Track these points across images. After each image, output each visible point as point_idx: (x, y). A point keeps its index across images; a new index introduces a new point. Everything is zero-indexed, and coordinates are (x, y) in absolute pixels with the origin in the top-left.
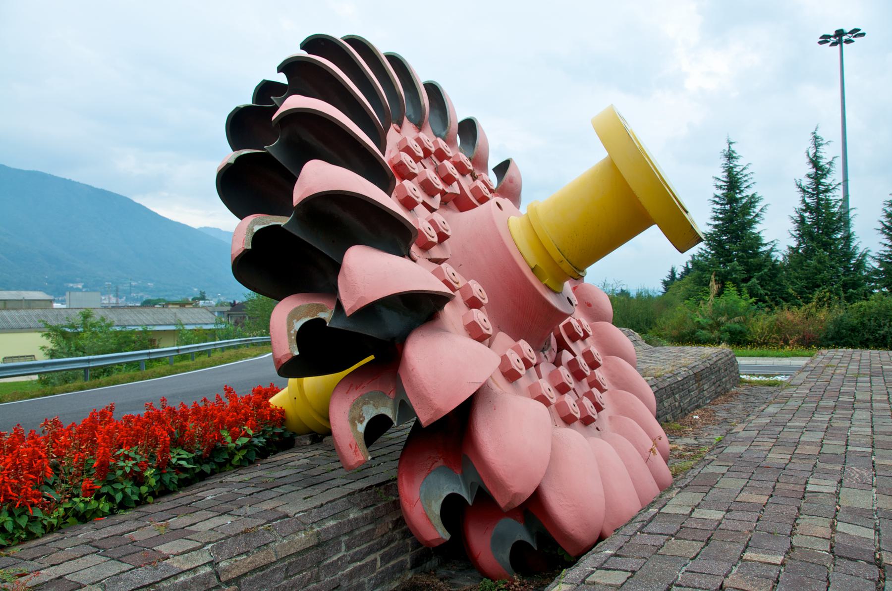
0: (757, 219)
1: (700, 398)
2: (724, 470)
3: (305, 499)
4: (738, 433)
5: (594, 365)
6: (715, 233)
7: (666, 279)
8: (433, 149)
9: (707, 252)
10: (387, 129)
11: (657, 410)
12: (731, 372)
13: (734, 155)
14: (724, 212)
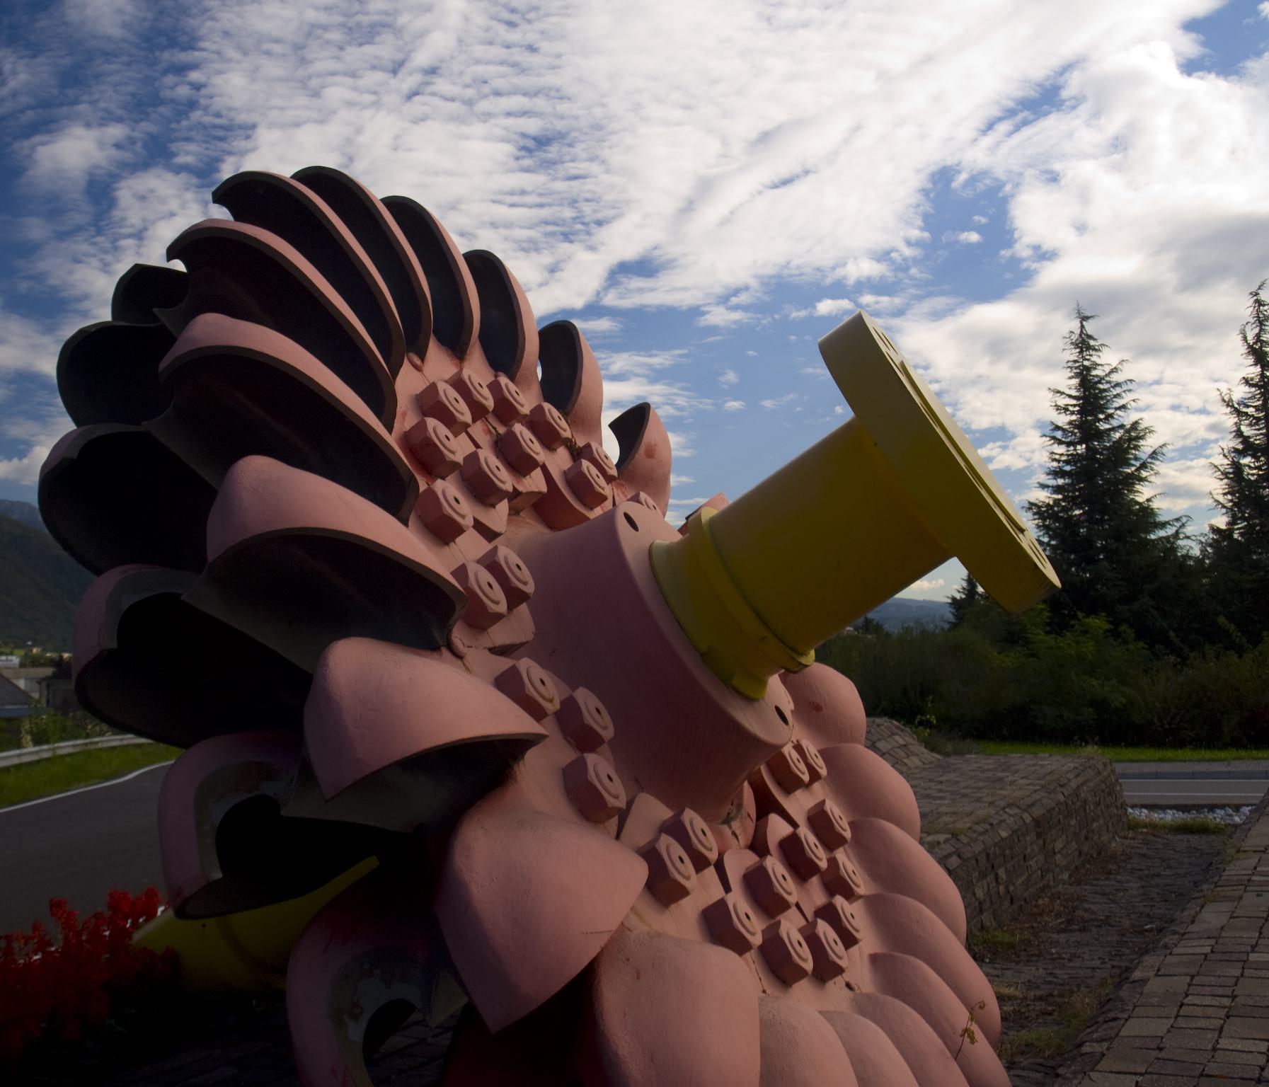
0: (1144, 474)
4: (1144, 981)
5: (830, 839)
6: (1056, 502)
7: (958, 596)
8: (490, 403)
10: (395, 372)
12: (1108, 807)
13: (1092, 343)
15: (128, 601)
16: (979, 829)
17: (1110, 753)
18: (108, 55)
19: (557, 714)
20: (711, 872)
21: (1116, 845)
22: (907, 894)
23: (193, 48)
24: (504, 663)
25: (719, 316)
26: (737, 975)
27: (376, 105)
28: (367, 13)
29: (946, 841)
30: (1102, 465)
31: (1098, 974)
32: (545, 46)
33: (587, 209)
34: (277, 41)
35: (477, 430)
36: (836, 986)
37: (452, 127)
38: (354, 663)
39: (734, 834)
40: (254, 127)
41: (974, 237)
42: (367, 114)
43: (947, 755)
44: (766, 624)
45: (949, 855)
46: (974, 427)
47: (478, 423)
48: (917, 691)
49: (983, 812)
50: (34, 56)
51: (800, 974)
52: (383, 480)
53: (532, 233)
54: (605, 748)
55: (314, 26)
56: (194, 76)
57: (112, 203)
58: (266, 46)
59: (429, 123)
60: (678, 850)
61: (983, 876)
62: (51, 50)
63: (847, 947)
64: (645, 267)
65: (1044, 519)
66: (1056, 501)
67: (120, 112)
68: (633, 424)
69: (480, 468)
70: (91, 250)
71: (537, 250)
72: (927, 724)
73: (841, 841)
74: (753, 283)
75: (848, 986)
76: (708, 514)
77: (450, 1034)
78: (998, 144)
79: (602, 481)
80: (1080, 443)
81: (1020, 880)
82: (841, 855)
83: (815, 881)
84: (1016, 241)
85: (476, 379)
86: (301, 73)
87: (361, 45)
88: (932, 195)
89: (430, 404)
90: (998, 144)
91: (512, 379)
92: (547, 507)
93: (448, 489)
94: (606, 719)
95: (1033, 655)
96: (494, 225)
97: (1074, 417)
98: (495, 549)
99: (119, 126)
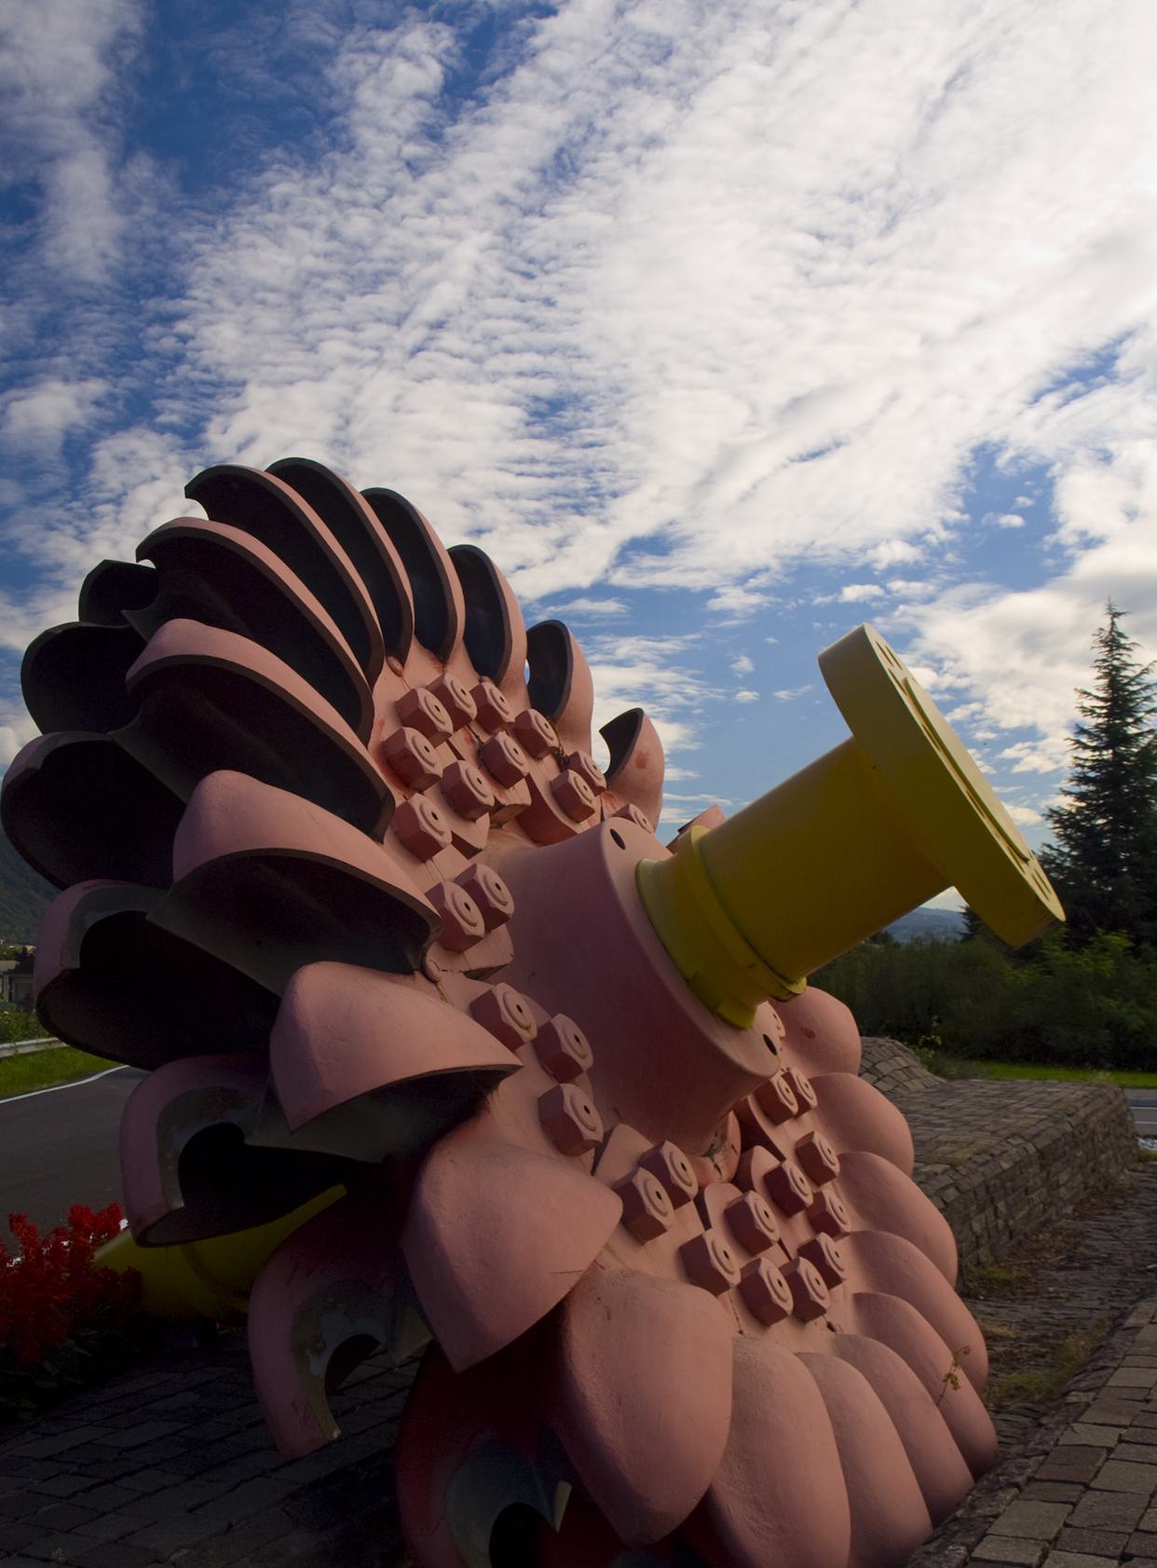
1: (1051, 1204)
2: (1110, 1438)
3: (191, 1511)
4: (1137, 1328)
6: (1080, 810)
8: (473, 711)
9: (1062, 854)
10: (372, 679)
11: (962, 1270)
13: (1123, 641)
14: (1098, 765)
15: (90, 920)
16: (979, 1159)
17: (1126, 1078)
18: (88, 302)
19: (534, 1042)
20: (690, 1208)
21: (1124, 1178)
22: (889, 1229)
23: (182, 296)
24: (480, 988)
25: (734, 599)
26: (715, 1316)
27: (378, 362)
28: (371, 260)
29: (944, 1172)
30: (1130, 771)
31: (1097, 1315)
32: (563, 299)
33: (603, 479)
34: (273, 289)
35: (459, 739)
36: (817, 1327)
37: (460, 387)
38: (323, 990)
39: (716, 1167)
40: (244, 383)
41: (1017, 521)
42: (368, 371)
43: (951, 1078)
44: (755, 951)
45: (947, 1187)
46: (1003, 725)
47: (460, 731)
48: (919, 1012)
49: (985, 1141)
50: (10, 303)
51: (781, 1314)
52: (358, 799)
53: (535, 505)
54: (583, 1078)
55: (312, 274)
56: (182, 327)
57: (89, 465)
58: (260, 295)
59: (435, 381)
60: (656, 1185)
61: (982, 1209)
62: (29, 296)
63: (830, 1286)
64: (656, 545)
65: (1065, 828)
66: (1079, 809)
67: (101, 366)
68: (624, 731)
69: (461, 781)
70: (66, 516)
71: (545, 522)
72: (931, 1045)
73: (829, 1175)
74: (774, 564)
75: (830, 1326)
76: (698, 833)
77: (417, 1365)
78: (1044, 419)
79: (589, 793)
80: (1106, 748)
81: (1021, 1214)
82: (828, 1191)
83: (800, 1217)
84: (1060, 526)
85: (459, 686)
86: (297, 325)
87: (363, 294)
88: (973, 473)
89: (410, 713)
90: (1044, 419)
91: (497, 684)
92: (532, 821)
93: (426, 804)
94: (585, 1047)
95: (1049, 973)
96: (499, 495)
97: (1101, 720)
98: (474, 867)
99: (100, 381)
